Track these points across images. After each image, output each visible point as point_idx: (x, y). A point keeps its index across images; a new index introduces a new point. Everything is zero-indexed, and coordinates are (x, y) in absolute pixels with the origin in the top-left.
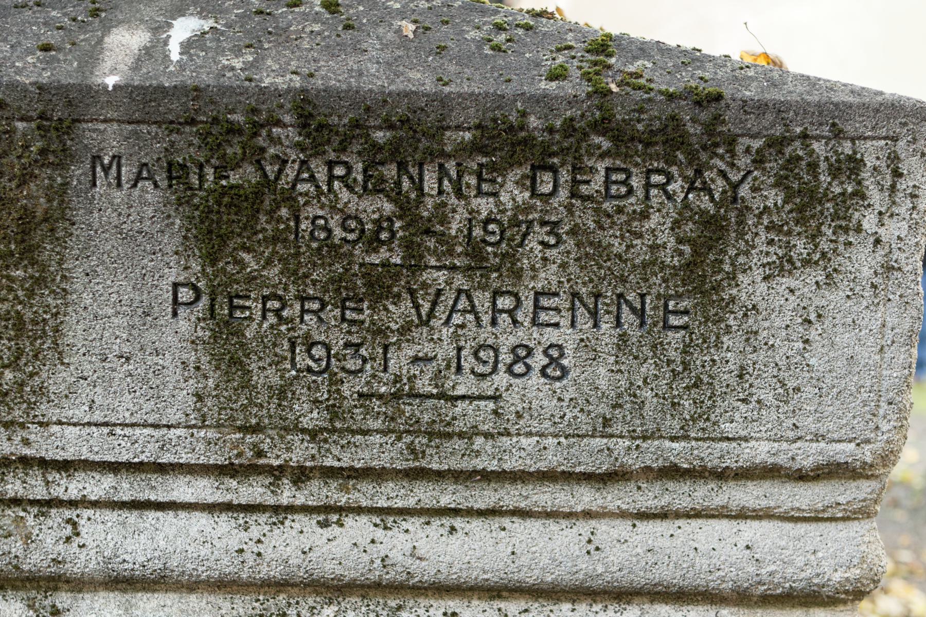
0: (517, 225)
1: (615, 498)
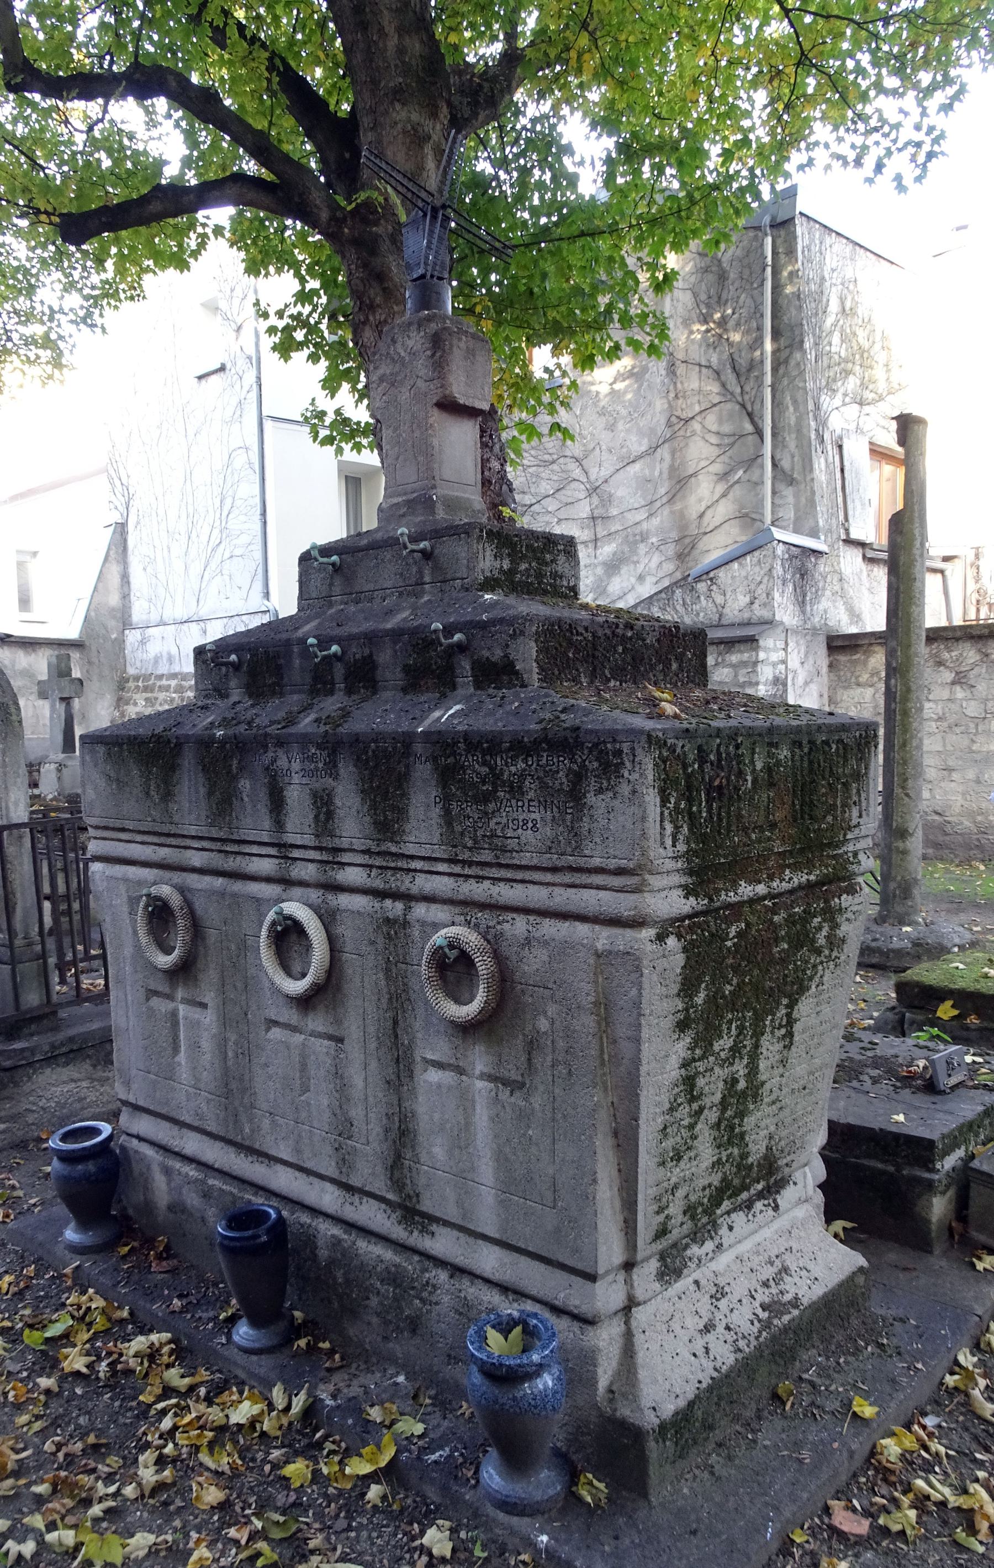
0: (522, 776)
1: (557, 878)
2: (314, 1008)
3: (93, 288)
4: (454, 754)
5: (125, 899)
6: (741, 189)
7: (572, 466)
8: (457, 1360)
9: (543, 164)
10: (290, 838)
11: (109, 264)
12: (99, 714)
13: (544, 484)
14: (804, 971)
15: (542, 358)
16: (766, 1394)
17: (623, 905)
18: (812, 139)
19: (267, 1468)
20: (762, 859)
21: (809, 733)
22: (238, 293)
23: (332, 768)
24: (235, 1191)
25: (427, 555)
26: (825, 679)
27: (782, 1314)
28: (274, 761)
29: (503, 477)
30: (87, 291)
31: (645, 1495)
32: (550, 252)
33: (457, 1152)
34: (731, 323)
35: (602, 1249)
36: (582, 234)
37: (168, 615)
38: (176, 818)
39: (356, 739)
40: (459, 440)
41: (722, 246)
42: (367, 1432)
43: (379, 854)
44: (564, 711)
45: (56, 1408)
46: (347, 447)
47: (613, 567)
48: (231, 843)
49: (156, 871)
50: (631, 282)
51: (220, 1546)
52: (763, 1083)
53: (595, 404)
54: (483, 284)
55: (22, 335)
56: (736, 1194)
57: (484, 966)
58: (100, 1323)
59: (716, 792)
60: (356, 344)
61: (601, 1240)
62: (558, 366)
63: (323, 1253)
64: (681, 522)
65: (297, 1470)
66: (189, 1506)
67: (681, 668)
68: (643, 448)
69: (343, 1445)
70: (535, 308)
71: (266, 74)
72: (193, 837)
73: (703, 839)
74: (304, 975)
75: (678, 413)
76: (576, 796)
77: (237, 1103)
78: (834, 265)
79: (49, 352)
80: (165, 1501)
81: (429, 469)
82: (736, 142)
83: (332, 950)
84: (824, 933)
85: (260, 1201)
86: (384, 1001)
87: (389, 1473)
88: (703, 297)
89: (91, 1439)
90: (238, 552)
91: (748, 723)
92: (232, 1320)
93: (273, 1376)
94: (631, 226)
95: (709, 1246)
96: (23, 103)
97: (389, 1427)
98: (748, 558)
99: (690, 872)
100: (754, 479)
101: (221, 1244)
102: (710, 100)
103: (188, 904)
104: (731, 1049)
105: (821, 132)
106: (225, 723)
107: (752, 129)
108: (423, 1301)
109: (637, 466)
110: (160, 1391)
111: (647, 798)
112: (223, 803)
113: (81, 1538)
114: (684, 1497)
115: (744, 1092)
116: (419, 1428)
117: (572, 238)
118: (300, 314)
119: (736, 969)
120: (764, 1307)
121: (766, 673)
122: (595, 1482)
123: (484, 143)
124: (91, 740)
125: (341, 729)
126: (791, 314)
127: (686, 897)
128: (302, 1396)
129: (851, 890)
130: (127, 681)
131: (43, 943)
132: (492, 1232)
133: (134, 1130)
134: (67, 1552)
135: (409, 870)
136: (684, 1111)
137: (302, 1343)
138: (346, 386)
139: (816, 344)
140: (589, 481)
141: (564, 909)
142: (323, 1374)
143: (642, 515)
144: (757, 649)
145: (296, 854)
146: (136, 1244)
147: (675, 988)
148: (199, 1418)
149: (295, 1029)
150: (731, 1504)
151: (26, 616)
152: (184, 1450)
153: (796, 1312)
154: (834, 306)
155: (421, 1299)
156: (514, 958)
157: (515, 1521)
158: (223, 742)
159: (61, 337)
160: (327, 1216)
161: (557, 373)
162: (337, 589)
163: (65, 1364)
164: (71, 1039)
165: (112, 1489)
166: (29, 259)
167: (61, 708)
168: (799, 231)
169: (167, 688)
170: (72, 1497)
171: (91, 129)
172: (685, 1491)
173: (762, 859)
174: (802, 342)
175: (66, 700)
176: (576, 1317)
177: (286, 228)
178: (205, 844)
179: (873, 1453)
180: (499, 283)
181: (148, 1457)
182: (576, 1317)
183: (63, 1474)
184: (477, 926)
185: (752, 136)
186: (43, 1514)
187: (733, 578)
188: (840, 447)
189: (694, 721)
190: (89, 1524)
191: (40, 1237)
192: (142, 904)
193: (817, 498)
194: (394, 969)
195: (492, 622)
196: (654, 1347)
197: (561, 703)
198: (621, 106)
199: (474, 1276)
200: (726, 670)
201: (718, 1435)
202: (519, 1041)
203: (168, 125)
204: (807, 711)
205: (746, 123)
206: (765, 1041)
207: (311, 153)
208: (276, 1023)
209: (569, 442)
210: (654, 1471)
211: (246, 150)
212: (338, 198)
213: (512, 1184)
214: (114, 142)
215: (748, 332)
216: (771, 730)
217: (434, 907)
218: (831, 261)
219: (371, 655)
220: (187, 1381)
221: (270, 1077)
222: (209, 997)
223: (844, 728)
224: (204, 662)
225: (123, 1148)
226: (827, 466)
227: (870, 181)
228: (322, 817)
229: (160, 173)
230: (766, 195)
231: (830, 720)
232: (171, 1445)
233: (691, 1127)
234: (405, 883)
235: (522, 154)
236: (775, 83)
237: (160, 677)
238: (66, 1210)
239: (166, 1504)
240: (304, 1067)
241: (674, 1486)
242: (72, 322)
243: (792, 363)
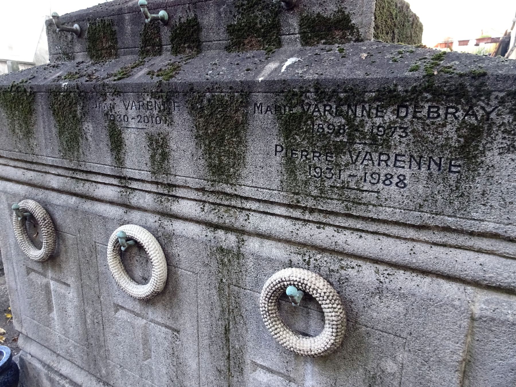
0: (391, 128)
1: (423, 235)
4: (301, 103)
10: (129, 173)
23: (166, 114)
28: (112, 108)
38: (36, 150)
39: (190, 89)
43: (212, 192)
57: (332, 312)
72: (51, 166)
86: (217, 312)
106: (70, 76)
125: (173, 80)
145: (135, 185)
156: (361, 303)
158: (68, 91)
178: (60, 171)
208: (122, 308)
217: (267, 243)
219: (196, 18)
221: (120, 343)
228: (158, 157)
234: (240, 220)
240: (146, 342)
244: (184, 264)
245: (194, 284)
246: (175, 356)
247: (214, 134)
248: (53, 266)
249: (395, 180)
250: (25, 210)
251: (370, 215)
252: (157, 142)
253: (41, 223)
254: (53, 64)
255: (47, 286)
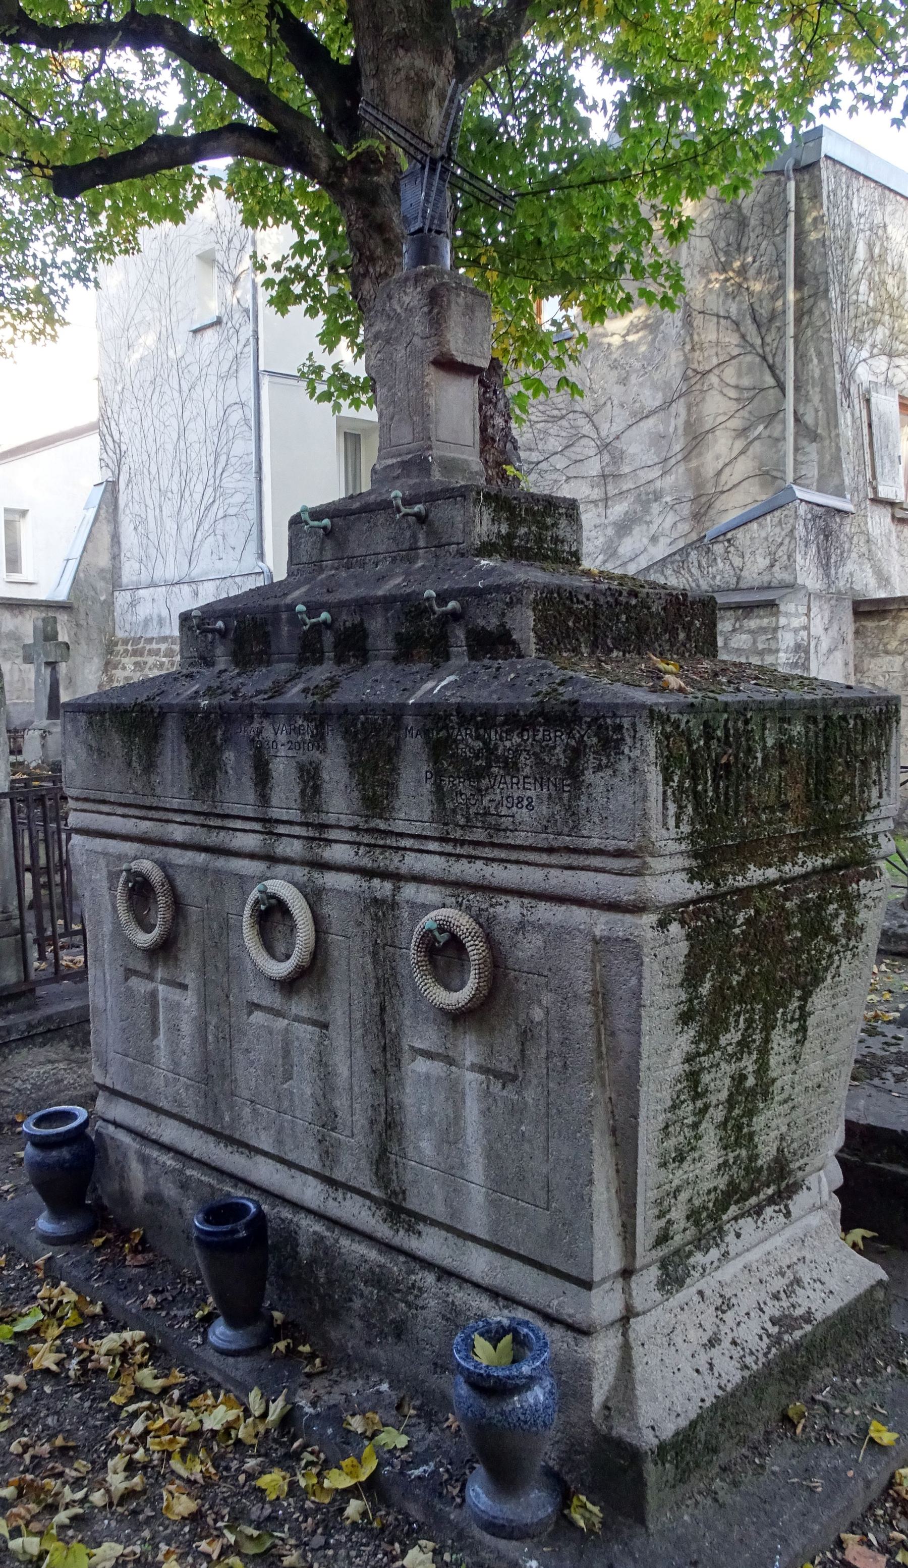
0: (517, 751)
1: (554, 859)
2: (298, 992)
3: (87, 241)
4: (446, 727)
5: (104, 872)
6: (761, 132)
7: (582, 421)
8: (444, 1369)
9: (554, 110)
10: (275, 813)
11: (103, 217)
12: (86, 680)
13: (552, 440)
14: (818, 961)
15: (550, 309)
16: (775, 1415)
17: (622, 888)
18: (837, 79)
19: (242, 1478)
20: (773, 841)
21: (824, 708)
22: (236, 243)
23: (319, 740)
24: (214, 1182)
25: (421, 519)
26: (851, 646)
27: (794, 1329)
28: (259, 732)
29: (507, 435)
30: (80, 244)
31: (641, 1520)
32: (559, 200)
33: (445, 1146)
34: (752, 272)
35: (598, 1255)
36: (593, 181)
37: (158, 575)
38: (159, 791)
39: (345, 714)
40: (456, 401)
41: (742, 192)
42: (349, 1443)
43: (367, 831)
44: (563, 683)
45: (24, 1407)
46: (345, 403)
47: (624, 527)
48: (216, 818)
49: (136, 845)
50: (643, 231)
51: (190, 1559)
52: (774, 1080)
53: (607, 357)
54: (488, 234)
55: (13, 290)
56: (744, 1198)
57: (475, 950)
58: (72, 1317)
59: (723, 771)
60: (355, 297)
61: (597, 1245)
62: (567, 318)
63: (305, 1252)
64: (697, 480)
65: (273, 1481)
66: (159, 1516)
67: (688, 638)
68: (657, 403)
69: (322, 1456)
70: (543, 259)
71: (266, 22)
73: (709, 819)
74: (288, 957)
75: (695, 366)
76: (573, 773)
77: (216, 1090)
78: (862, 209)
79: (40, 307)
80: (135, 1509)
81: (426, 429)
82: (756, 84)
83: (317, 931)
84: (841, 920)
85: (240, 1193)
86: (371, 986)
87: (371, 1488)
88: (722, 244)
89: (59, 1441)
90: (232, 511)
91: (758, 697)
92: (209, 1319)
93: (249, 1380)
94: (644, 172)
95: (714, 1253)
96: (18, 54)
97: (371, 1439)
98: (768, 518)
99: (695, 855)
100: (776, 434)
101: (197, 1238)
102: (728, 41)
103: (170, 880)
104: (739, 1043)
105: (846, 72)
106: (210, 692)
107: (774, 69)
108: (409, 1305)
109: (651, 421)
110: (130, 1392)
111: (649, 777)
112: (207, 776)
113: (46, 1546)
114: (684, 1525)
115: (753, 1090)
116: (402, 1441)
117: (584, 186)
118: (298, 266)
119: (745, 959)
120: (774, 1321)
121: (787, 640)
122: (589, 1505)
123: (490, 88)
124: (78, 707)
125: (329, 701)
126: (814, 264)
127: (691, 881)
128: (280, 1401)
129: (871, 875)
130: (116, 644)
131: (22, 918)
132: (483, 1234)
133: (110, 1116)
134: (30, 1561)
135: (398, 849)
136: (688, 1109)
137: (281, 1345)
138: (344, 341)
139: (843, 293)
140: (599, 438)
141: (559, 892)
142: (303, 1379)
143: (656, 472)
144: (777, 614)
145: (281, 829)
146: (111, 1235)
147: (678, 978)
148: (171, 1422)
149: (278, 1014)
150: (735, 1535)
151: (15, 577)
152: (156, 1456)
153: (808, 1328)
154: (861, 252)
155: (406, 1302)
157: (503, 1544)
158: (207, 712)
159: (53, 292)
160: (309, 1211)
161: (565, 326)
162: (328, 554)
163: (34, 1361)
164: (49, 1018)
165: (80, 1495)
166: (22, 212)
167: (46, 672)
168: (824, 175)
169: (157, 653)
170: (38, 1503)
171: (87, 79)
172: (686, 1518)
173: (773, 841)
174: (827, 291)
175: (52, 665)
176: (570, 1327)
177: (285, 177)
179: (891, 1484)
180: (505, 233)
181: (117, 1462)
182: (570, 1327)
183: (29, 1477)
184: (469, 908)
185: (773, 78)
186: (7, 1519)
187: (752, 539)
188: (868, 401)
189: (700, 695)
190: (54, 1531)
191: (12, 1226)
192: (122, 880)
193: (843, 454)
194: (382, 953)
195: (488, 590)
196: (654, 1362)
197: (559, 675)
198: (635, 48)
199: (463, 1280)
200: (744, 637)
201: (722, 1458)
202: (512, 1031)
203: (166, 74)
204: (824, 684)
205: (767, 64)
206: (776, 1035)
207: (312, 101)
208: (258, 1007)
209: (577, 397)
210: (652, 1497)
211: (244, 100)
212: (338, 147)
213: (502, 1183)
214: (111, 91)
215: (770, 281)
216: (783, 704)
217: (424, 887)
218: (858, 206)
220: (160, 1382)
221: (252, 1062)
222: (190, 978)
223: (863, 702)
224: (190, 628)
225: (99, 1134)
226: (854, 422)
227: (897, 122)
228: (309, 791)
229: (157, 125)
230: (788, 140)
231: (847, 694)
232: (141, 1450)
233: (695, 1126)
234: (393, 862)
235: (532, 99)
236: (798, 22)
237: (150, 640)
238: (40, 1198)
239: (135, 1513)
241: (672, 1512)
242: (64, 276)
243: (817, 313)
244: (335, 927)
245: (346, 953)
246: (322, 1062)
247: (368, 761)
248: (166, 961)
249: (525, 803)
250: (138, 874)
251: (509, 841)
252: (308, 772)
253: (159, 890)
254: (185, 672)
255: (154, 994)
